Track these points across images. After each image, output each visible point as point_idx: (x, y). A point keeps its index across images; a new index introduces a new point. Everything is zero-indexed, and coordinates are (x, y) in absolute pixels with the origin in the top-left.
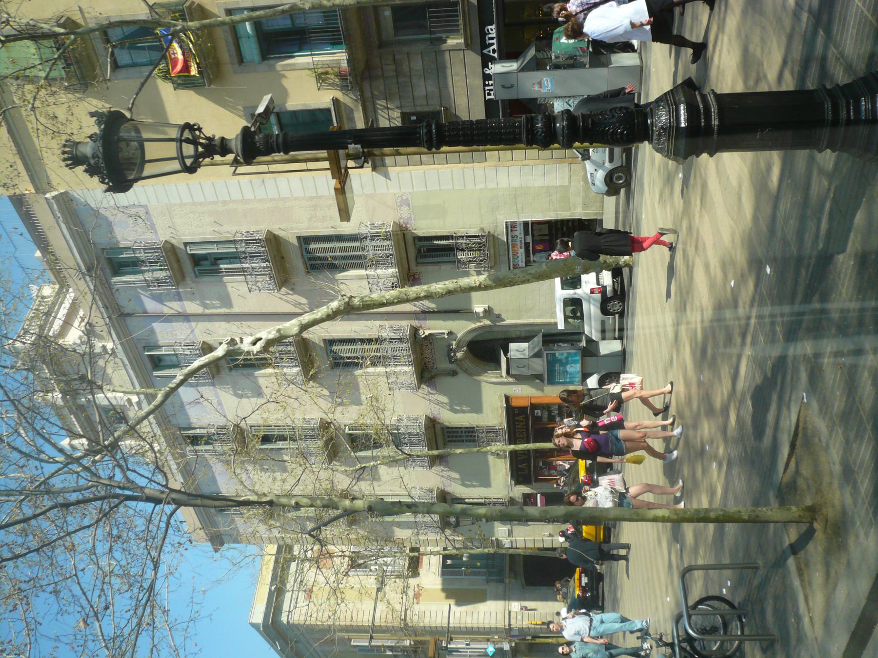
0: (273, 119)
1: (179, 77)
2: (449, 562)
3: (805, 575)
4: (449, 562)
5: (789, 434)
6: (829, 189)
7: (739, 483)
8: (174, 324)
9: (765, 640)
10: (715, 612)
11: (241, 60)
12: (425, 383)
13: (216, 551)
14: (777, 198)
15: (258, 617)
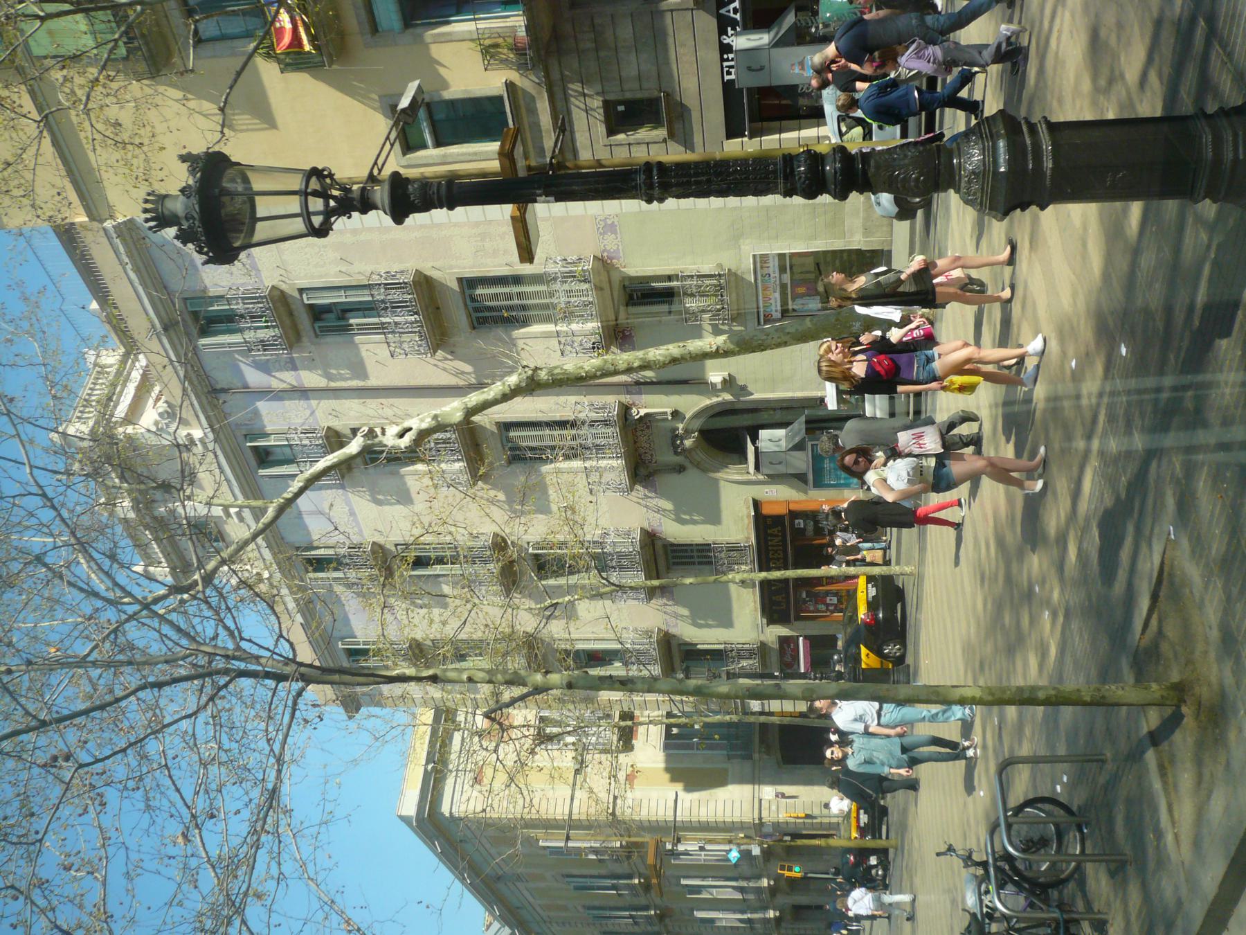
0: (422, 113)
1: (288, 54)
2: (675, 731)
3: (1170, 775)
4: (675, 731)
5: (1150, 583)
6: (1209, 247)
7: (1080, 642)
8: (287, 403)
9: (1114, 861)
10: (1051, 819)
11: (374, 28)
12: (640, 483)
13: (350, 718)
14: (1136, 252)
15: (409, 806)
